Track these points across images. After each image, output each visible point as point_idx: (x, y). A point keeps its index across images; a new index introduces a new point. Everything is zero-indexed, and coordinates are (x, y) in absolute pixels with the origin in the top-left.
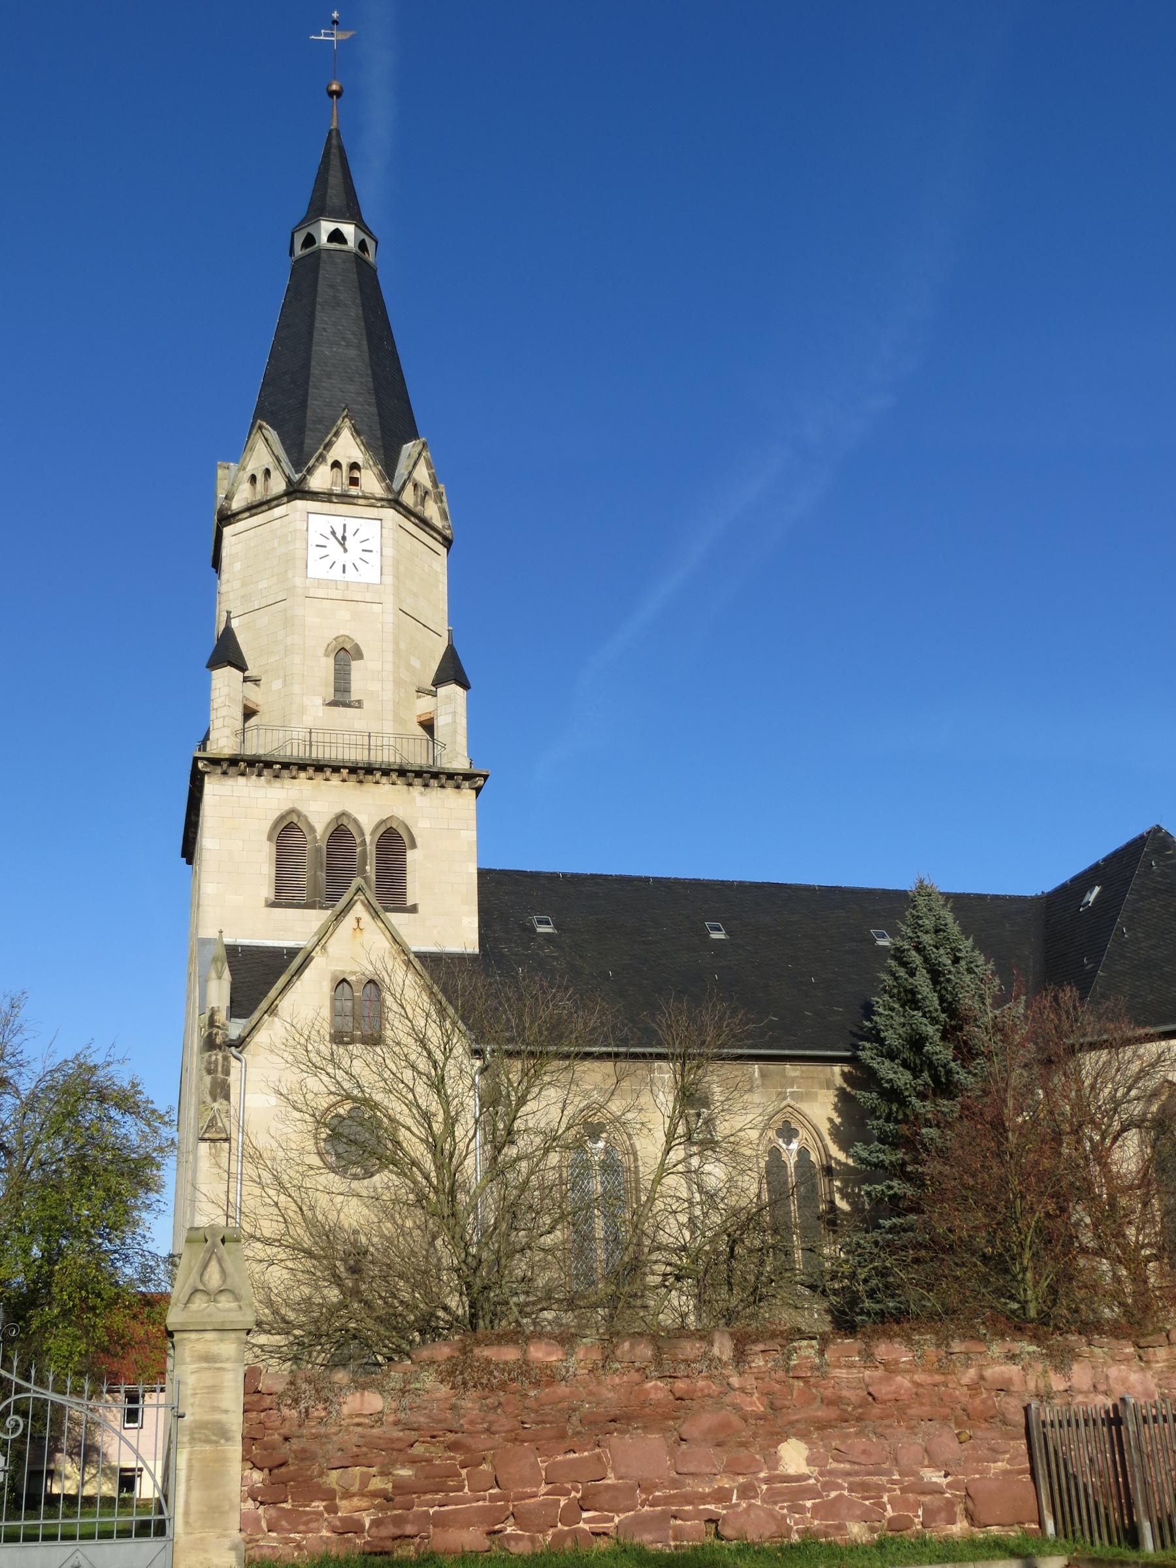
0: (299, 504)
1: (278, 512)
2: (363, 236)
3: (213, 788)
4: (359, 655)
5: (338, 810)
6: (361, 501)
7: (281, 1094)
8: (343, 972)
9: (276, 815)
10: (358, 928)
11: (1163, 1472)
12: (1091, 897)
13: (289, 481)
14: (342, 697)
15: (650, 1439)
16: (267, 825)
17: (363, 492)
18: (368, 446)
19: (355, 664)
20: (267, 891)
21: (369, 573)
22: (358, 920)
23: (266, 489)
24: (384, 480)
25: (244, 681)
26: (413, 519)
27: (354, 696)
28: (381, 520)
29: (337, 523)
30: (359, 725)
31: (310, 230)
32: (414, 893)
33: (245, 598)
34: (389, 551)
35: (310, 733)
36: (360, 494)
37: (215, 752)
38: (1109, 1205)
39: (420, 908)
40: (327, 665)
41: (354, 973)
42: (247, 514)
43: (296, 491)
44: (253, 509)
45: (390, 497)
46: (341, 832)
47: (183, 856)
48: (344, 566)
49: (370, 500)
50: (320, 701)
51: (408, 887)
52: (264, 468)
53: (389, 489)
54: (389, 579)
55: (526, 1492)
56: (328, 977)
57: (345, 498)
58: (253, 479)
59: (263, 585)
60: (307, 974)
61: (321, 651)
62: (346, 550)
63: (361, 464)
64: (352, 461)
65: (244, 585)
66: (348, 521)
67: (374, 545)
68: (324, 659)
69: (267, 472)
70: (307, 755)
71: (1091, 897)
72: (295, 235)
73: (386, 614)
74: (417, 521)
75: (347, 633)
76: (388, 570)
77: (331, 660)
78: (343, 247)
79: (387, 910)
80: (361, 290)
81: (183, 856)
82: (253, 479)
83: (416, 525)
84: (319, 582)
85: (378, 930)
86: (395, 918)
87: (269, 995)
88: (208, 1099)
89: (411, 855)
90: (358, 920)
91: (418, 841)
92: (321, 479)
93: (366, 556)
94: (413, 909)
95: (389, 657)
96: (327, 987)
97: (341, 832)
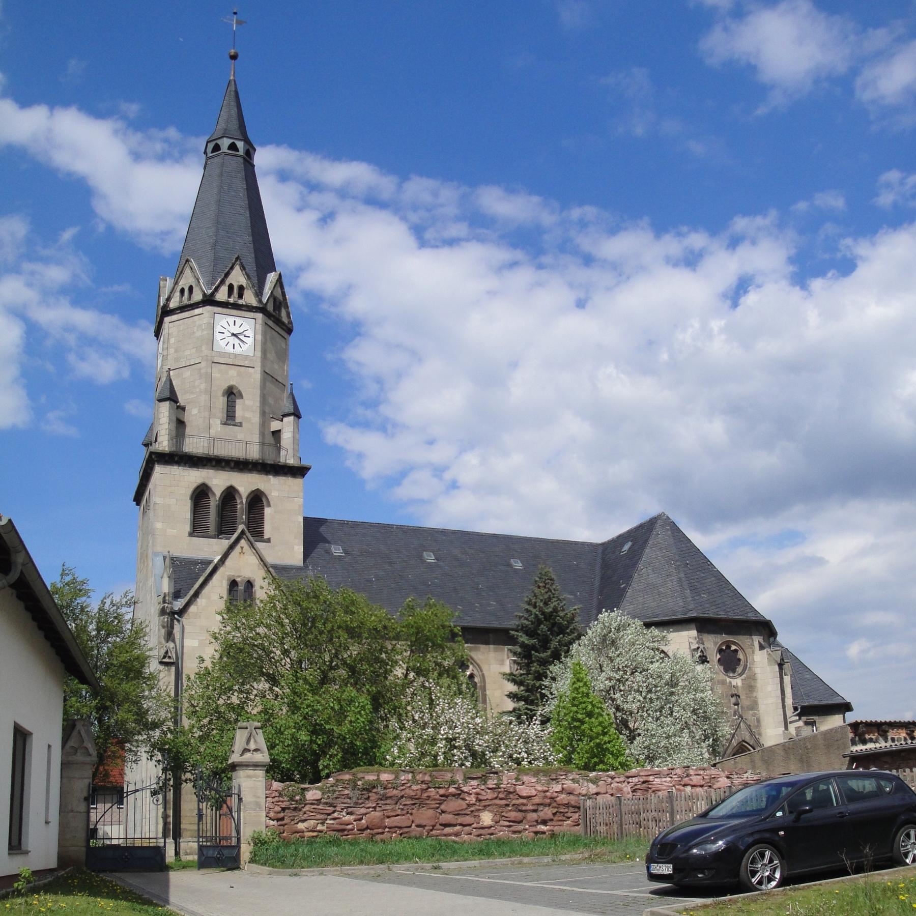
0: (208, 308)
1: (197, 311)
2: (248, 147)
5: (228, 484)
9: (195, 486)
10: (242, 553)
11: (609, 839)
12: (626, 547)
13: (204, 294)
16: (190, 492)
18: (249, 277)
19: (238, 401)
20: (188, 528)
22: (242, 548)
23: (190, 298)
24: (258, 296)
25: (177, 408)
27: (238, 420)
30: (240, 437)
31: (219, 142)
32: (268, 531)
33: (177, 360)
34: (259, 337)
35: (214, 440)
36: (244, 303)
37: (161, 449)
39: (272, 541)
40: (221, 402)
41: (239, 576)
43: (209, 301)
44: (182, 309)
45: (261, 306)
46: (230, 494)
47: (134, 501)
48: (235, 325)
50: (219, 422)
53: (260, 301)
54: (259, 354)
58: (182, 291)
59: (187, 353)
63: (245, 286)
64: (240, 284)
65: (176, 351)
69: (191, 288)
70: (212, 452)
71: (626, 547)
72: (209, 144)
73: (256, 375)
76: (259, 348)
78: (238, 153)
79: (256, 541)
80: (247, 181)
81: (134, 501)
82: (182, 291)
85: (252, 554)
86: (259, 545)
88: (163, 641)
89: (267, 511)
90: (242, 548)
91: (272, 503)
94: (268, 540)
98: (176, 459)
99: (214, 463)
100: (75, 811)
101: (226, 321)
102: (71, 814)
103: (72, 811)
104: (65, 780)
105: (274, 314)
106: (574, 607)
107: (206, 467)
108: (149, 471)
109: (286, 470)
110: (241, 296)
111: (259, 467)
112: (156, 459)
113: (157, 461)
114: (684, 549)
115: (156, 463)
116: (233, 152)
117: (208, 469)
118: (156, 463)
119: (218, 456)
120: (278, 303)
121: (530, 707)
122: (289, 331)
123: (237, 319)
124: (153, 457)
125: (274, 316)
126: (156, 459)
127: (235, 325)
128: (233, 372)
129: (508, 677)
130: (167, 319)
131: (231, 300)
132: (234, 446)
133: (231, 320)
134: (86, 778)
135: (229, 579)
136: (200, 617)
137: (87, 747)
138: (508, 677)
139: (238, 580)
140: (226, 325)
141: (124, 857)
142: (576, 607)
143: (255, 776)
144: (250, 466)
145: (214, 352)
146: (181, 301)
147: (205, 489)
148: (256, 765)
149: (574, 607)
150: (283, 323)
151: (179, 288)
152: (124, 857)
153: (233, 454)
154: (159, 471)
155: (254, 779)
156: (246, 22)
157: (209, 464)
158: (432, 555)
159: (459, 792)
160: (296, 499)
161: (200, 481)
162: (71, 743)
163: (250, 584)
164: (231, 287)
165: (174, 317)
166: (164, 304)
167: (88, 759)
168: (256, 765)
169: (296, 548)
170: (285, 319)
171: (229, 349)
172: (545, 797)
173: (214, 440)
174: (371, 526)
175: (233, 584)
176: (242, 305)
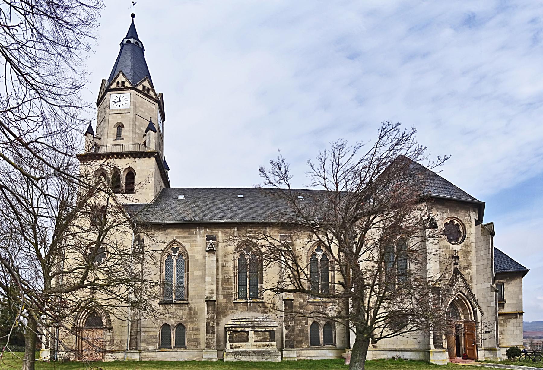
4: (123, 126)
7: (359, 163)
14: (119, 136)
15: (477, 296)
21: (127, 106)
29: (118, 96)
49: (127, 89)
54: (132, 107)
55: (300, 311)
61: (113, 127)
66: (121, 95)
67: (128, 99)
68: (114, 129)
75: (120, 121)
76: (132, 104)
77: (116, 129)
87: (303, 359)
93: (126, 102)
95: (132, 126)
97: (116, 171)
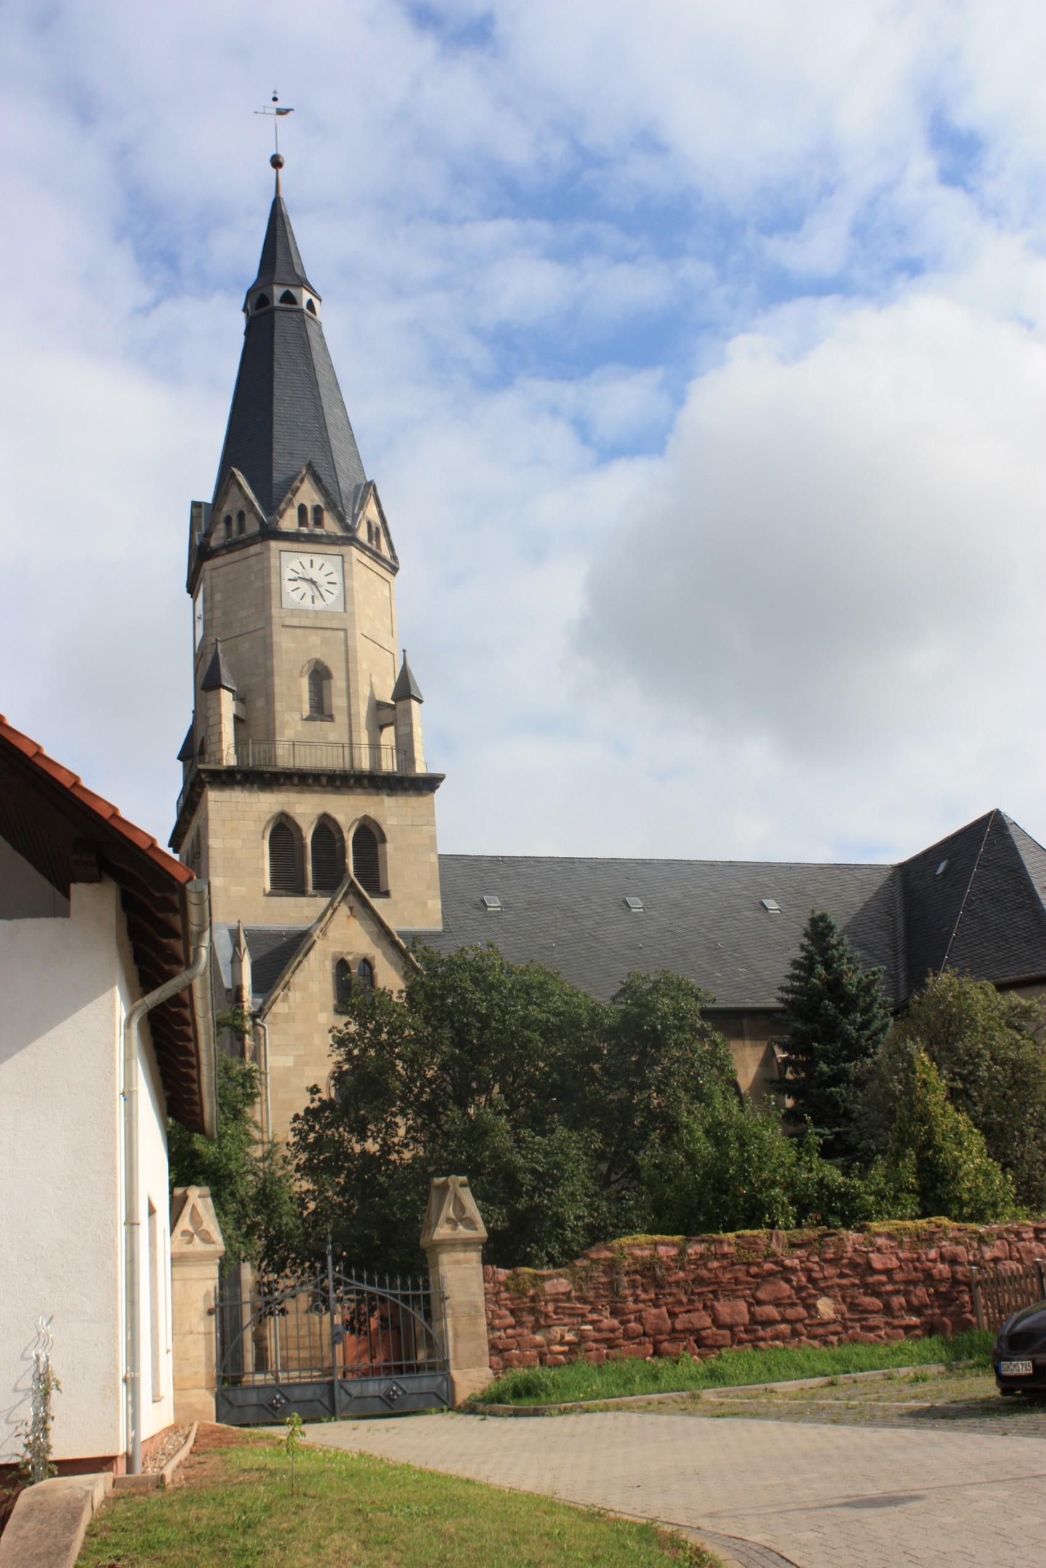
1: (253, 550)
3: (215, 800)
6: (324, 540)
8: (341, 953)
17: (326, 531)
26: (367, 553)
28: (342, 556)
35: (294, 745)
36: (324, 533)
38: (967, 1055)
41: (350, 953)
42: (224, 551)
44: (230, 547)
46: (326, 827)
48: (312, 566)
51: (330, 1424)
52: (238, 510)
56: (330, 957)
57: (312, 539)
60: (312, 954)
62: (292, 110)
63: (323, 506)
74: (370, 555)
83: (369, 557)
84: (293, 612)
86: (376, 903)
92: (289, 522)
96: (329, 967)
97: (326, 827)
98: (239, 777)
99: (296, 780)
100: (195, 1331)
101: (298, 561)
102: (190, 1337)
103: (191, 1333)
104: (177, 1284)
105: (369, 545)
106: (873, 969)
107: (284, 787)
108: (195, 799)
109: (407, 784)
110: (318, 522)
111: (366, 782)
112: (207, 780)
113: (209, 783)
114: (1038, 865)
115: (208, 786)
116: (289, 306)
117: (287, 791)
118: (208, 786)
119: (302, 770)
120: (374, 529)
121: (819, 1130)
122: (394, 570)
123: (315, 558)
124: (203, 776)
125: (369, 550)
126: (207, 780)
127: (312, 566)
128: (315, 639)
129: (778, 1086)
130: (207, 565)
131: (304, 530)
132: (324, 752)
133: (306, 559)
134: (208, 1279)
135: (334, 958)
136: (294, 1019)
137: (209, 1230)
138: (778, 1086)
139: (349, 958)
140: (299, 569)
141: (274, 1401)
142: (875, 969)
143: (467, 1261)
144: (352, 781)
145: (283, 611)
146: (229, 534)
147: (284, 820)
148: (466, 1244)
149: (873, 969)
150: (384, 560)
151: (222, 516)
152: (274, 1401)
153: (324, 765)
154: (215, 800)
155: (465, 1265)
156: (292, 110)
157: (288, 782)
158: (640, 902)
159: (781, 1269)
160: (425, 828)
161: (277, 809)
162: (185, 1223)
163: (367, 964)
164: (302, 510)
165: (218, 561)
166: (201, 543)
167: (210, 1248)
168: (466, 1244)
169: (430, 903)
170: (385, 552)
171: (307, 603)
172: (916, 1269)
173: (294, 745)
174: (540, 862)
175: (342, 966)
176: (321, 536)
